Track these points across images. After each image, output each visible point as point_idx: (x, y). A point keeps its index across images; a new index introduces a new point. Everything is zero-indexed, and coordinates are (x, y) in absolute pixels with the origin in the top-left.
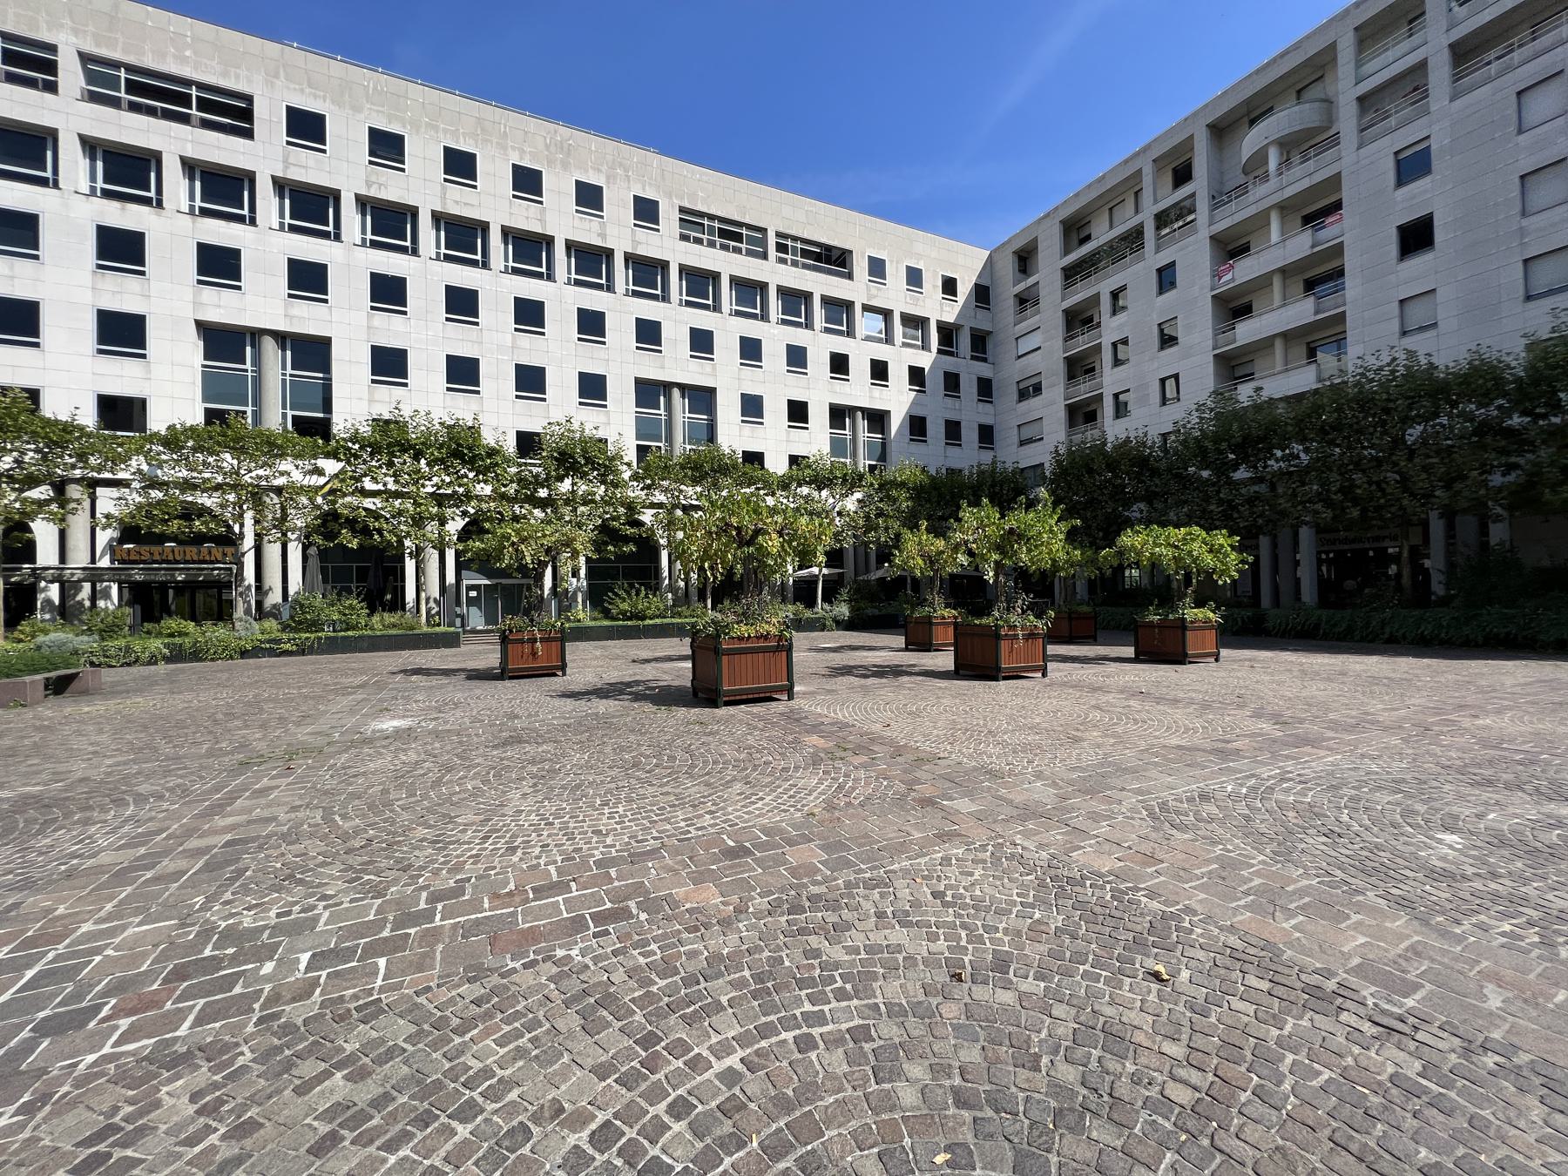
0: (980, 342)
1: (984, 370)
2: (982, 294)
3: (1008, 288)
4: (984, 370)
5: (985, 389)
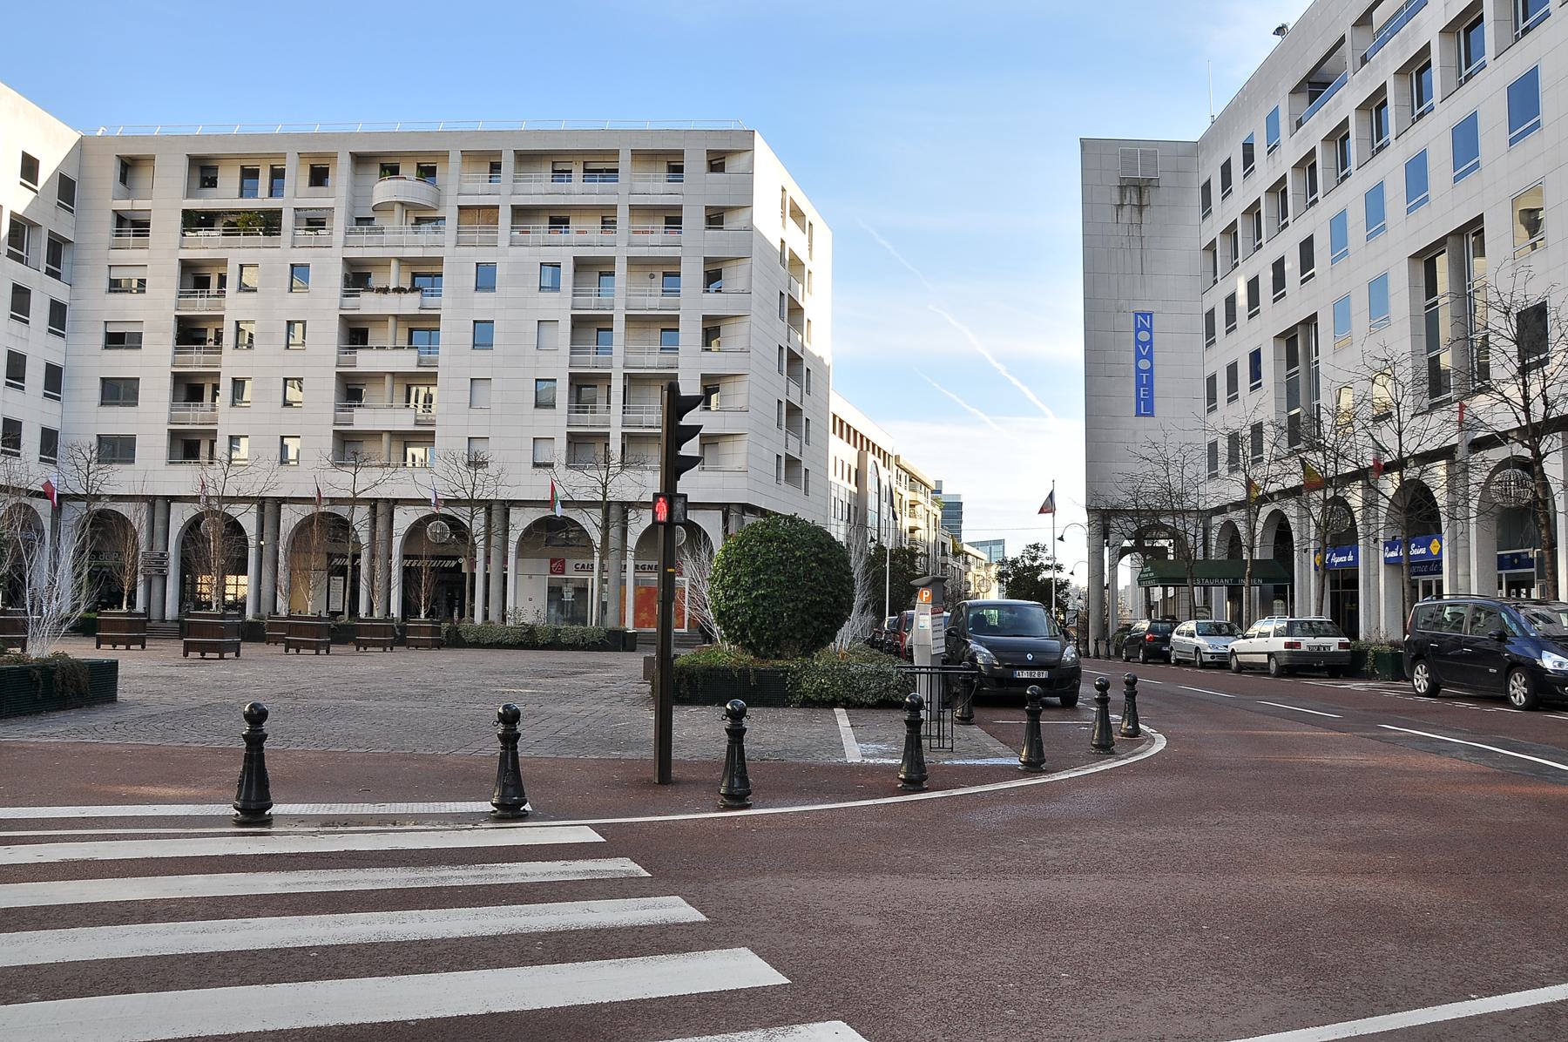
0: (57, 246)
1: (58, 290)
2: (66, 188)
3: (105, 197)
4: (58, 290)
5: (58, 313)
